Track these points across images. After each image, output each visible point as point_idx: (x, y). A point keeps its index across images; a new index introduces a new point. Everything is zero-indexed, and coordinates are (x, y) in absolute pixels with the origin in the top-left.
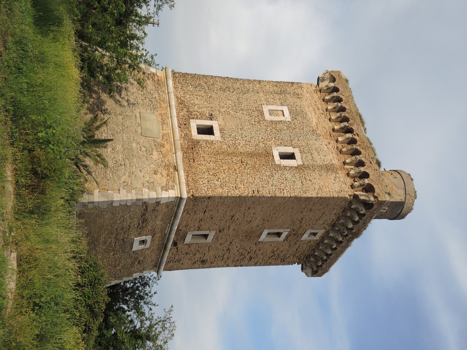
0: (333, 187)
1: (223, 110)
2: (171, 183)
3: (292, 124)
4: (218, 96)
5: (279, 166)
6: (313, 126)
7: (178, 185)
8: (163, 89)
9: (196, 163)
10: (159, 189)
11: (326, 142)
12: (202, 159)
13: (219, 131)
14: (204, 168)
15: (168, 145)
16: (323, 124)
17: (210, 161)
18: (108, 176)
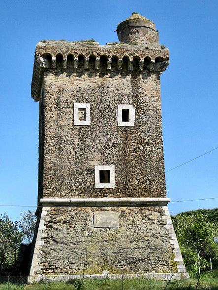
5: (135, 124)
11: (109, 80)
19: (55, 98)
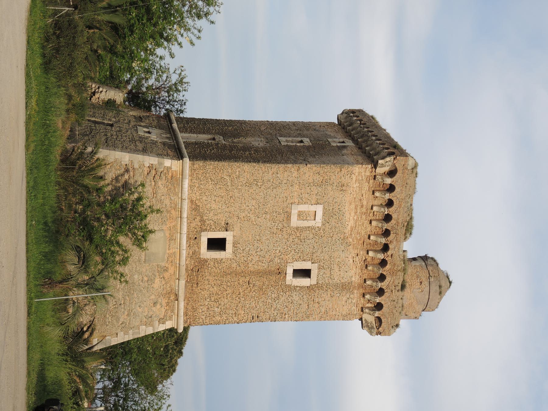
0: (341, 310)
1: (242, 215)
2: (169, 313)
3: (321, 231)
4: (241, 194)
5: (289, 286)
6: (346, 231)
7: (176, 316)
8: (176, 190)
9: (199, 288)
10: (157, 323)
11: (353, 252)
12: (206, 282)
13: (232, 245)
14: (206, 293)
15: (173, 268)
16: (360, 228)
17: (215, 285)
18: (107, 320)
19: (332, 179)
